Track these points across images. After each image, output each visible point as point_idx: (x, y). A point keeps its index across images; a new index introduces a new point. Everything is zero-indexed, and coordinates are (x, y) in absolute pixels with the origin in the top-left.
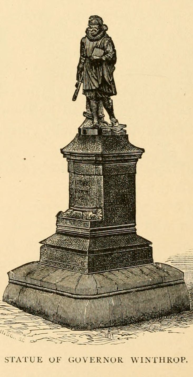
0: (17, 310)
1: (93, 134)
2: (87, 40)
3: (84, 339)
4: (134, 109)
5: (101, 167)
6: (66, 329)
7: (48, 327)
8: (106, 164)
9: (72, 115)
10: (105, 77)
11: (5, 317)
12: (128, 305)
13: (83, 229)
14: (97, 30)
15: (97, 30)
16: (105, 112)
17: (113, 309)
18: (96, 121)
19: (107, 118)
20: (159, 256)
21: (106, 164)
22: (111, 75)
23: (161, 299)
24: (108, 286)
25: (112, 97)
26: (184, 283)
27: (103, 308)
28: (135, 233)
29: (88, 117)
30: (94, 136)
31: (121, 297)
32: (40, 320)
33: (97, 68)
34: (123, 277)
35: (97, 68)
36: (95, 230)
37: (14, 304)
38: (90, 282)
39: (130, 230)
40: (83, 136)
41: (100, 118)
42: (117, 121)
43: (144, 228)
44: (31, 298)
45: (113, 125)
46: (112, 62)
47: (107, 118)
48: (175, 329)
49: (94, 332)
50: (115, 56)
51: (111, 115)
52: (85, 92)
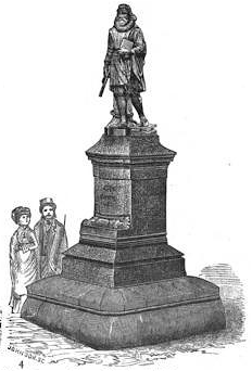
0: (36, 327)
1: (113, 255)
2: (114, 31)
3: (110, 360)
4: (164, 109)
5: (129, 171)
6: (90, 349)
7: (70, 346)
8: (134, 161)
9: (100, 112)
10: (135, 71)
11: (23, 335)
12: (158, 323)
13: (111, 237)
14: (125, 11)
15: (125, 11)
16: (134, 111)
17: (142, 326)
18: (124, 120)
19: (136, 117)
20: (192, 269)
21: (134, 161)
22: (141, 70)
23: (193, 316)
24: (137, 303)
25: (141, 94)
26: (219, 299)
27: (132, 324)
28: (166, 243)
29: (116, 114)
30: (121, 137)
31: (151, 314)
32: (61, 339)
33: (125, 65)
34: (152, 292)
35: (125, 65)
36: (122, 240)
37: (33, 320)
38: (118, 297)
39: (161, 240)
40: (109, 135)
41: (129, 117)
42: (146, 121)
43: (175, 238)
44: (52, 313)
45: (142, 125)
46: (141, 55)
47: (136, 117)
48: (208, 350)
49: (121, 353)
50: (145, 49)
51: (141, 113)
52: (112, 88)
